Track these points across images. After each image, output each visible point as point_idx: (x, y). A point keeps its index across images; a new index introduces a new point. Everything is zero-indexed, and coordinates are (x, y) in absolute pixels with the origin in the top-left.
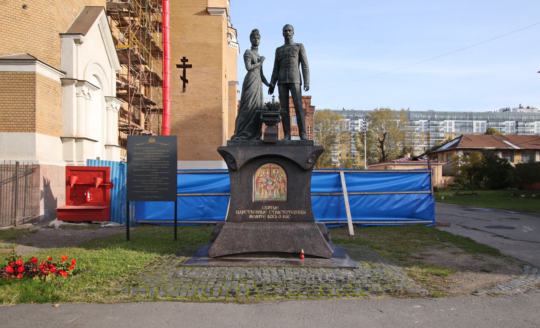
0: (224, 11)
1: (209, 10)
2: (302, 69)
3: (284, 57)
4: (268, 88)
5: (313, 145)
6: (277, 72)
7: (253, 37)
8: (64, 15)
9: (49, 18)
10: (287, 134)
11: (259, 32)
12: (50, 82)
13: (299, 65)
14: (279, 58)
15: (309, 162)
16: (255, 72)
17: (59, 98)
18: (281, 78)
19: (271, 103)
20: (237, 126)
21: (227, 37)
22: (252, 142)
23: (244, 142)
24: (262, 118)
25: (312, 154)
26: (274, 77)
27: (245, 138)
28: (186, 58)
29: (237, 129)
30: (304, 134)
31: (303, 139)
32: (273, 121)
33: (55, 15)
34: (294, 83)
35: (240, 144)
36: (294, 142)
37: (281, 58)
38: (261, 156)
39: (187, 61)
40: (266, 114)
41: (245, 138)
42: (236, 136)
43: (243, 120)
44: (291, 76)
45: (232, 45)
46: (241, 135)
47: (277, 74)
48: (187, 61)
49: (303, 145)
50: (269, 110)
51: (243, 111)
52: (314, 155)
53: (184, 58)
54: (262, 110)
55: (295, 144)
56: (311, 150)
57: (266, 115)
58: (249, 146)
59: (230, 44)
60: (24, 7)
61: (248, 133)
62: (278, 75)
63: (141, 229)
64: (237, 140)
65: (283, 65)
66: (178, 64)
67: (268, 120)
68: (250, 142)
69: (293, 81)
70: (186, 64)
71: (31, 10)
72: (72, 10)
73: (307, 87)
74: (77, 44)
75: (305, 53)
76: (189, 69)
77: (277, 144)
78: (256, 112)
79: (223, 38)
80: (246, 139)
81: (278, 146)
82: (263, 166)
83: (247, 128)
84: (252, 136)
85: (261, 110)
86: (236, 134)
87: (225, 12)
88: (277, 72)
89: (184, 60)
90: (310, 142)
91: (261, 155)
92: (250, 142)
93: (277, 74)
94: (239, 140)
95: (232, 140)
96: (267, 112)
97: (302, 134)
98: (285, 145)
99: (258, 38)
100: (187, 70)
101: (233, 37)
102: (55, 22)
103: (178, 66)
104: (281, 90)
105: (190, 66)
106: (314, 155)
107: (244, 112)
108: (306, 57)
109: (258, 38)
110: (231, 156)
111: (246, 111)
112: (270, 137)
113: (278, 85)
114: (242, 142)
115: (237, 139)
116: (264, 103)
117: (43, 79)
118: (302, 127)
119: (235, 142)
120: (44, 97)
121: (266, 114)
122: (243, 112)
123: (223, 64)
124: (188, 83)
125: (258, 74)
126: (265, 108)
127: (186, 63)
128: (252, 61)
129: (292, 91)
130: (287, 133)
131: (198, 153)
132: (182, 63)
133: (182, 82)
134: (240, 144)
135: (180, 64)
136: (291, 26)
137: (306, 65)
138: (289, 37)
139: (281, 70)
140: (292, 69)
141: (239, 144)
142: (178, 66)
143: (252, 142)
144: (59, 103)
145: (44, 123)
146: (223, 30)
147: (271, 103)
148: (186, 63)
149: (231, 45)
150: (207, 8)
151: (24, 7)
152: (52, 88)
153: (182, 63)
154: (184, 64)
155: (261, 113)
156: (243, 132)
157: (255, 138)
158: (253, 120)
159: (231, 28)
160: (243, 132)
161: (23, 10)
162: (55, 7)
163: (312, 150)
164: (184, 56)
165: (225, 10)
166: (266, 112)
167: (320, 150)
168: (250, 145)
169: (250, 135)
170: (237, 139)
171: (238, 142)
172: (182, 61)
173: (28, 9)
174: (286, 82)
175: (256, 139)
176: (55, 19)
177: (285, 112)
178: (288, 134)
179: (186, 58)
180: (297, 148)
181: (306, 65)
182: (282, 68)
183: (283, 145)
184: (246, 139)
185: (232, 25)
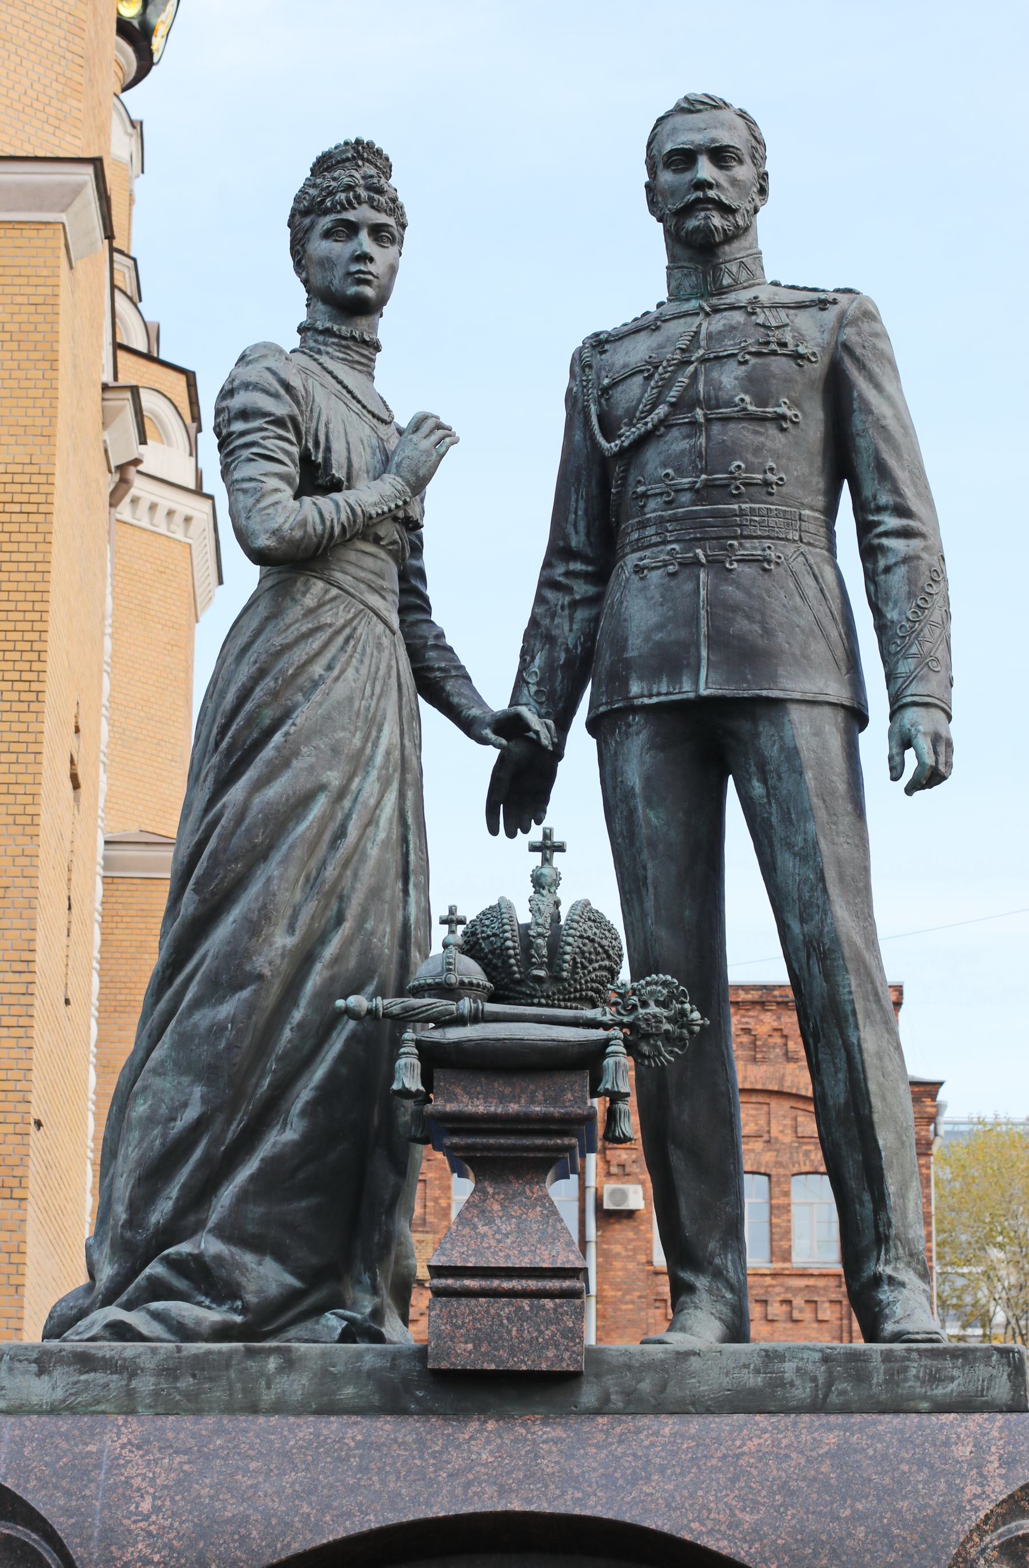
0: (77, 190)
2: (869, 552)
3: (664, 423)
4: (491, 755)
6: (582, 589)
7: (326, 222)
10: (701, 1282)
11: (386, 170)
13: (831, 511)
14: (609, 432)
16: (338, 576)
18: (636, 646)
19: (524, 916)
20: (123, 1186)
21: (105, 425)
22: (290, 1363)
23: (199, 1365)
24: (414, 1083)
26: (550, 639)
27: (215, 1316)
29: (121, 1212)
30: (907, 1275)
31: (897, 1337)
32: (545, 1126)
34: (778, 704)
35: (145, 1384)
36: (789, 1368)
37: (629, 434)
40: (454, 1034)
41: (215, 1316)
42: (108, 1300)
43: (191, 1114)
44: (742, 625)
45: (153, 507)
46: (158, 1290)
47: (581, 614)
49: (897, 1408)
50: (493, 999)
51: (197, 1004)
54: (418, 992)
55: (802, 1392)
56: (993, 1466)
57: (458, 1045)
58: (253, 1409)
59: (135, 501)
61: (248, 1258)
62: (596, 619)
63: (756, 1279)
64: (109, 1348)
65: (653, 509)
67: (479, 1107)
68: (272, 1364)
69: (772, 679)
73: (924, 744)
75: (889, 387)
77: (588, 1395)
78: (349, 1013)
79: (61, 426)
80: (222, 1333)
81: (598, 1412)
83: (243, 1197)
84: (292, 1297)
85: (400, 993)
86: (107, 1272)
87: (91, 191)
88: (582, 589)
90: (982, 1371)
91: (393, 1518)
92: (272, 1364)
93: (581, 614)
94: (131, 1349)
95: (54, 1344)
96: (477, 1018)
97: (877, 1280)
98: (683, 1408)
99: (378, 232)
101: (164, 438)
104: (634, 776)
107: (204, 1018)
108: (908, 429)
109: (378, 232)
110: (33, 1538)
111: (226, 1009)
112: (504, 1308)
113: (593, 726)
114: (169, 1371)
115: (120, 1331)
116: (438, 910)
118: (880, 1200)
119: (85, 1362)
121: (454, 1034)
122: (197, 1016)
123: (49, 657)
125: (374, 600)
126: (449, 967)
128: (306, 460)
129: (758, 788)
130: (697, 1266)
134: (145, 1384)
136: (742, 115)
137: (914, 504)
138: (717, 221)
139: (632, 559)
140: (752, 548)
141: (130, 1393)
143: (290, 1363)
146: (64, 348)
147: (524, 916)
149: (143, 506)
155: (404, 1019)
156: (185, 1248)
157: (333, 1322)
158: (310, 1110)
160: (185, 1248)
165: (87, 173)
166: (460, 1021)
168: (267, 1397)
169: (273, 1290)
170: (120, 1331)
171: (130, 1369)
174: (686, 690)
175: (346, 1337)
177: (680, 1019)
178: (718, 1274)
180: (832, 1439)
181: (902, 511)
182: (639, 546)
183: (660, 1408)
184: (222, 1333)
185: (153, 333)
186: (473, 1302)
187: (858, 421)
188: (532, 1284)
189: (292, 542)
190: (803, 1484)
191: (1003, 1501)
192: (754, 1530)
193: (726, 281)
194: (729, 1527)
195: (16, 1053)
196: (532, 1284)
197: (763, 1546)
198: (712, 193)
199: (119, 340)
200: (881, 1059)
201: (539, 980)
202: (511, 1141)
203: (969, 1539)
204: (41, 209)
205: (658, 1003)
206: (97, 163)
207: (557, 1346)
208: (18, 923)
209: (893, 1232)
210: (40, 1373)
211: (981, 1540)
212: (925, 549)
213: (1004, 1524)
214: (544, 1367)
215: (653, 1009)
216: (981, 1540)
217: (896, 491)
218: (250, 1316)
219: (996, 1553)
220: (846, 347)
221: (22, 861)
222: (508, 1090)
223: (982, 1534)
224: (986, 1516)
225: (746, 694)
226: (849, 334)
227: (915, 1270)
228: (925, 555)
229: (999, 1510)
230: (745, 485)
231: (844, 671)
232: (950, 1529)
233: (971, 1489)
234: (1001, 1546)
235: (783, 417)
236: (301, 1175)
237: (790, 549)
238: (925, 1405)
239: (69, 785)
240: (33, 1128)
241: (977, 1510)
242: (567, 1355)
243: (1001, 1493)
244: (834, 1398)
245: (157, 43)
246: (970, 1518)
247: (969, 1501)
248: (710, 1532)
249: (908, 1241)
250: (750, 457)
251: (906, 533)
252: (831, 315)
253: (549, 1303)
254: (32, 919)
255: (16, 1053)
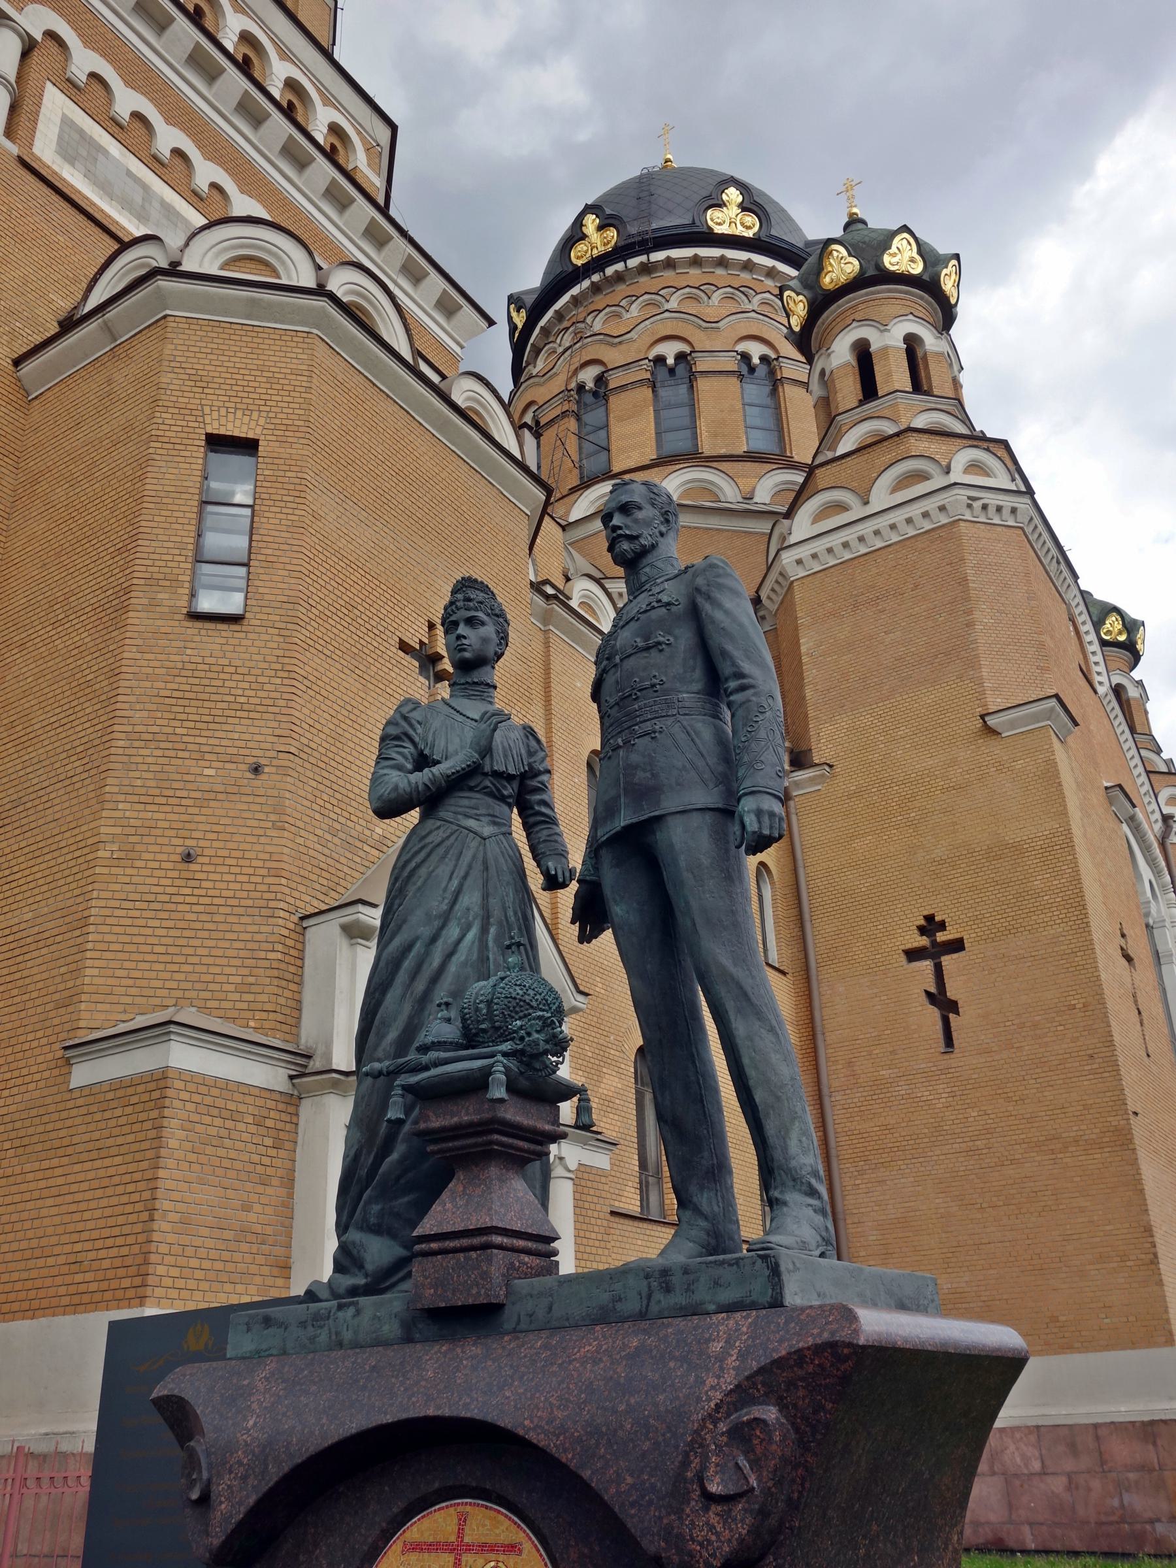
1: (992, 721)
5: (777, 1303)
8: (326, 851)
9: (264, 872)
12: (240, 1097)
15: (714, 1488)
17: (282, 1153)
25: (742, 1395)
28: (937, 919)
33: (285, 858)
38: (427, 1420)
39: (942, 926)
48: (942, 926)
52: (771, 1413)
53: (930, 918)
55: (632, 1305)
60: (188, 858)
66: (909, 946)
70: (938, 940)
71: (206, 860)
72: (367, 832)
74: (354, 941)
76: (955, 956)
82: (419, 1529)
87: (1059, 709)
89: (931, 925)
100: (949, 961)
102: (284, 881)
103: (913, 955)
105: (957, 946)
106: (771, 1413)
112: (450, 1261)
117: (203, 1089)
120: (204, 1159)
124: (957, 1013)
127: (941, 937)
131: (1054, 1319)
132: (924, 941)
133: (934, 1013)
135: (916, 945)
142: (913, 955)
144: (280, 1173)
145: (194, 1263)
148: (941, 937)
150: (982, 717)
151: (188, 858)
152: (250, 1119)
153: (924, 941)
154: (934, 943)
159: (1170, 773)
161: (184, 866)
162: (286, 834)
163: (742, 1356)
164: (926, 913)
165: (1053, 702)
167: (818, 1349)
172: (922, 930)
173: (200, 860)
176: (284, 873)
179: (937, 919)
186: (434, 1258)
187: (710, 628)
188: (465, 1242)
189: (390, 801)
190: (602, 1383)
191: (731, 1390)
192: (562, 1425)
193: (643, 579)
194: (547, 1423)
195: (1115, 1083)
196: (465, 1242)
197: (565, 1438)
198: (620, 532)
199: (1148, 769)
200: (752, 1040)
201: (484, 1031)
202: (457, 1143)
203: (703, 1427)
204: (1038, 722)
205: (538, 1032)
206: (1057, 696)
207: (477, 1285)
208: (1102, 1025)
209: (776, 1164)
210: (248, 1330)
211: (715, 1426)
212: (755, 694)
213: (736, 1411)
214: (470, 1301)
215: (536, 1036)
216: (715, 1426)
217: (734, 664)
218: (369, 1279)
219: (725, 1439)
220: (698, 590)
221: (1097, 997)
222: (455, 1108)
223: (715, 1422)
224: (716, 1405)
225: (642, 818)
226: (700, 581)
227: (800, 1191)
228: (754, 698)
229: (729, 1399)
230: (640, 691)
231: (711, 785)
232: (688, 1419)
233: (711, 1381)
234: (729, 1432)
235: (659, 643)
236: (402, 1181)
237: (670, 721)
238: (712, 1307)
239: (1124, 962)
240: (1132, 1116)
241: (709, 1400)
242: (483, 1291)
243: (730, 1384)
244: (654, 1308)
245: (1139, 647)
246: (703, 1408)
247: (706, 1392)
248: (534, 1429)
249: (790, 1169)
250: (641, 674)
251: (743, 688)
252: (688, 576)
253: (473, 1254)
254: (1108, 1022)
255: (1115, 1083)
